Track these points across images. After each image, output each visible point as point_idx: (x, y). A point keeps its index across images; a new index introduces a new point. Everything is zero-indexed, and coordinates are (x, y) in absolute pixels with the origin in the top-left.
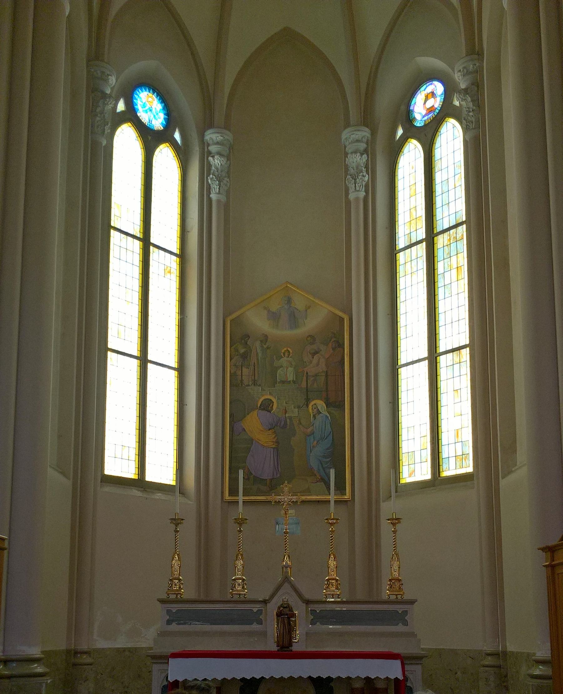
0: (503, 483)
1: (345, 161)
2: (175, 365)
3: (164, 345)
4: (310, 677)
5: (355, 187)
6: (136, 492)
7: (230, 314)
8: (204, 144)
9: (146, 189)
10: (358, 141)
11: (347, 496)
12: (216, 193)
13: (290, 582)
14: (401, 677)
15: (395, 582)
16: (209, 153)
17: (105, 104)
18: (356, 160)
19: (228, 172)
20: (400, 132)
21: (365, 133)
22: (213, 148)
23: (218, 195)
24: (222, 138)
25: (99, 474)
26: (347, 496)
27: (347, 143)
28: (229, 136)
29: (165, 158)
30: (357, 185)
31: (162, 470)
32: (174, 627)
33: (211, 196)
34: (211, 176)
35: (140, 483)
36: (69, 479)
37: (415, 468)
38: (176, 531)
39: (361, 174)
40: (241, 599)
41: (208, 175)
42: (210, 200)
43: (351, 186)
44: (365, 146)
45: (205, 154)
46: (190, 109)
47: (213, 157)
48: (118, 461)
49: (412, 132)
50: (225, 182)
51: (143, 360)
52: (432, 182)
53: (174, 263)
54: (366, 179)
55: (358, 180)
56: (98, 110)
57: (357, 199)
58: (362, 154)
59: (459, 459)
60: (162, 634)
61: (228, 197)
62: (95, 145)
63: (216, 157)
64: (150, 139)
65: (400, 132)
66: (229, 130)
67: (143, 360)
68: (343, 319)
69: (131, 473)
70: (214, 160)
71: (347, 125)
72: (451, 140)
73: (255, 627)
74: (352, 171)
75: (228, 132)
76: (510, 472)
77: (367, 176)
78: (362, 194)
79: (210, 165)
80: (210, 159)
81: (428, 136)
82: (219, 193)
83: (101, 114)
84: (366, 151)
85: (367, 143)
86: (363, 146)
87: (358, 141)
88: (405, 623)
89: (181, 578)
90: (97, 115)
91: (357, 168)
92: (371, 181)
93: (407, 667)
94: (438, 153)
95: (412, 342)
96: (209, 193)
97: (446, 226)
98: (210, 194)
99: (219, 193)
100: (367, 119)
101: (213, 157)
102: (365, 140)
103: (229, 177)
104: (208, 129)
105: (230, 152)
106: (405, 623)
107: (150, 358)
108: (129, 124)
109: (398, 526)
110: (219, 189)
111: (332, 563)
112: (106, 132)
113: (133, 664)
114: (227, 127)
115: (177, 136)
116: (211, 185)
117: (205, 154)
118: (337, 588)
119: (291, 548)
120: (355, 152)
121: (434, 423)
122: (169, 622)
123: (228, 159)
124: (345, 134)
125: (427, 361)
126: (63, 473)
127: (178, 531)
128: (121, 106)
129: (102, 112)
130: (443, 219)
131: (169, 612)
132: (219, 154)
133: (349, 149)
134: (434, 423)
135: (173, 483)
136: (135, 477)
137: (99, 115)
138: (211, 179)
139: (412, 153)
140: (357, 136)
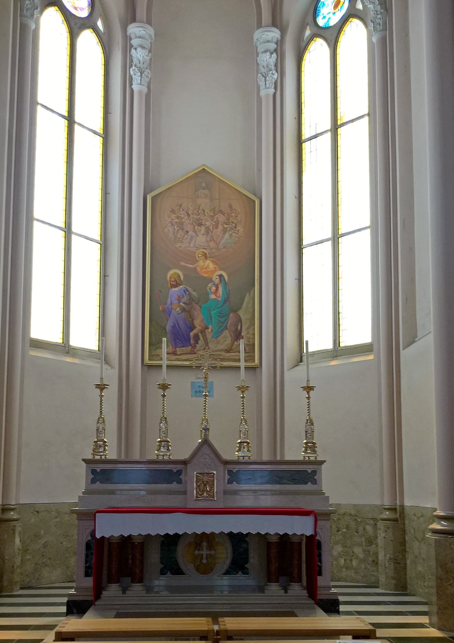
3: (88, 218)
5: (266, 84)
8: (127, 39)
9: (69, 71)
10: (268, 41)
13: (211, 446)
16: (131, 46)
18: (267, 60)
19: (150, 65)
21: (275, 34)
22: (135, 42)
23: (140, 86)
24: (144, 32)
28: (151, 31)
29: (88, 41)
30: (267, 82)
32: (98, 485)
33: (133, 87)
34: (134, 67)
36: (112, 367)
37: (318, 338)
38: (101, 396)
39: (271, 72)
41: (131, 66)
43: (262, 84)
44: (275, 46)
45: (127, 47)
47: (136, 49)
48: (44, 325)
52: (337, 80)
54: (275, 76)
55: (267, 78)
59: (359, 329)
60: (87, 492)
61: (149, 87)
62: (24, 28)
64: (75, 26)
65: (308, 33)
66: (151, 26)
68: (255, 201)
69: (57, 338)
70: (136, 51)
71: (259, 25)
72: (356, 39)
73: (174, 486)
74: (263, 70)
77: (276, 74)
79: (131, 56)
81: (332, 36)
82: (141, 84)
84: (276, 50)
85: (277, 43)
86: (273, 46)
87: (268, 41)
88: (315, 482)
89: (105, 440)
91: (267, 66)
93: (319, 523)
95: (316, 224)
96: (131, 84)
99: (141, 84)
100: (276, 22)
101: (136, 49)
102: (275, 40)
104: (130, 23)
108: (56, 8)
109: (311, 392)
110: (141, 80)
114: (149, 22)
115: (100, 24)
116: (133, 77)
119: (199, 412)
120: (265, 52)
121: (336, 296)
127: (103, 396)
130: (344, 114)
132: (143, 47)
134: (336, 296)
140: (268, 36)
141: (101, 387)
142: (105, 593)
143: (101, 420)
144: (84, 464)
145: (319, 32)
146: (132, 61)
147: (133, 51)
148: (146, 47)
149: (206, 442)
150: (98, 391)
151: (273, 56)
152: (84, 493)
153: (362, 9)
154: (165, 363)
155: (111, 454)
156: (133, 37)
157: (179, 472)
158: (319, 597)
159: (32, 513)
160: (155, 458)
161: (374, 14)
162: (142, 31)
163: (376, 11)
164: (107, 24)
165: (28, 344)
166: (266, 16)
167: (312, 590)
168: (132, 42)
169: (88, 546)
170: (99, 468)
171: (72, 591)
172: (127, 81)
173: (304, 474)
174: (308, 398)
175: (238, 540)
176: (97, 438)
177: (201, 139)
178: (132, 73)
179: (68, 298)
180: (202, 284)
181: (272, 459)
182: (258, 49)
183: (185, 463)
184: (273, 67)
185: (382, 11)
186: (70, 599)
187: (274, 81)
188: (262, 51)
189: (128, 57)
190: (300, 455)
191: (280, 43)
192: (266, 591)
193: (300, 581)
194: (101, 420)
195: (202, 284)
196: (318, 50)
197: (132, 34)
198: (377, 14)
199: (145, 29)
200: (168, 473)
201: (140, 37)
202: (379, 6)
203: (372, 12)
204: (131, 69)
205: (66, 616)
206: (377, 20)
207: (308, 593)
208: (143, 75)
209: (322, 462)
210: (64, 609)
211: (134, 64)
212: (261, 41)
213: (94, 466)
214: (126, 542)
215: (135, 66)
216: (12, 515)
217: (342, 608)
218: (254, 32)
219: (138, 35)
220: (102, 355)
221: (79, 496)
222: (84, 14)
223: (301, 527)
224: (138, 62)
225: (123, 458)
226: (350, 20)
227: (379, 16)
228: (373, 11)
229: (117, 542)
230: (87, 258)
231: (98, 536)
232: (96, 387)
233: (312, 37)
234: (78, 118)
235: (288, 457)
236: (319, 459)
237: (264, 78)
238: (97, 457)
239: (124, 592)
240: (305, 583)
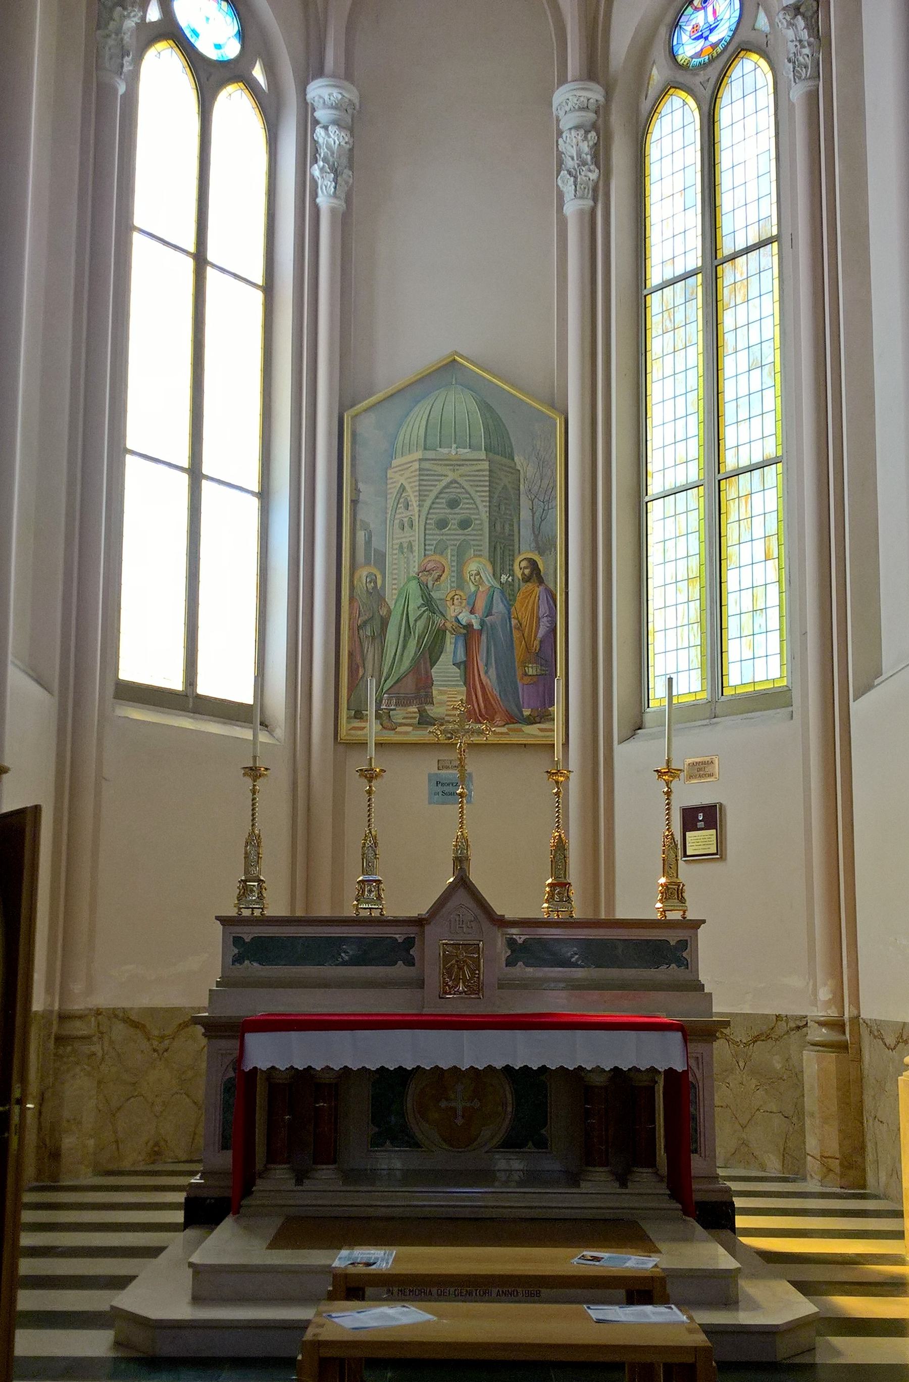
0: (855, 707)
3: (234, 449)
4: (508, 1069)
5: (576, 190)
8: (306, 110)
12: (330, 196)
14: (679, 1068)
15: (791, 25)
16: (316, 122)
17: (123, 18)
22: (322, 114)
23: (335, 201)
27: (561, 113)
29: (235, 106)
31: (228, 677)
33: (318, 200)
35: (187, 701)
37: (674, 664)
38: (254, 792)
41: (315, 161)
43: (568, 189)
45: (307, 122)
48: (146, 654)
49: (682, 77)
50: (344, 176)
52: (719, 167)
56: (112, 26)
64: (209, 77)
72: (751, 101)
73: (399, 970)
74: (570, 164)
76: (869, 687)
77: (597, 171)
79: (315, 142)
81: (706, 87)
82: (335, 195)
83: (117, 34)
84: (594, 126)
88: (683, 963)
90: (108, 36)
94: (725, 115)
96: (315, 195)
97: (741, 245)
98: (316, 196)
101: (326, 128)
102: (592, 107)
103: (351, 167)
105: (352, 119)
107: (206, 470)
110: (335, 188)
112: (125, 69)
115: (258, 73)
116: (320, 182)
117: (307, 122)
123: (351, 130)
126: (39, 681)
128: (154, 14)
129: (118, 31)
130: (737, 229)
131: (237, 941)
135: (250, 701)
137: (113, 36)
138: (322, 170)
139: (678, 114)
141: (253, 772)
142: (260, 1185)
143: (254, 841)
144: (219, 926)
145: (681, 77)
147: (319, 131)
149: (463, 883)
150: (249, 781)
151: (589, 136)
152: (218, 984)
155: (277, 905)
157: (409, 942)
158: (697, 1197)
160: (353, 913)
161: (796, 46)
163: (800, 41)
164: (271, 71)
165: (110, 690)
167: (679, 1183)
168: (317, 114)
169: (228, 1088)
170: (248, 934)
171: (196, 1180)
173: (665, 949)
174: (668, 794)
175: (528, 1082)
176: (245, 874)
177: (453, 301)
179: (198, 593)
181: (590, 916)
182: (561, 123)
183: (419, 922)
184: (589, 157)
185: (812, 39)
186: (192, 1195)
187: (591, 184)
188: (570, 125)
190: (655, 909)
191: (602, 110)
192: (583, 1184)
193: (651, 1162)
194: (254, 841)
196: (674, 130)
197: (316, 99)
198: (803, 47)
200: (386, 945)
203: (789, 43)
205: (185, 1229)
206: (801, 58)
207: (668, 1187)
209: (697, 924)
210: (179, 1217)
213: (239, 930)
214: (304, 1080)
216: (79, 1028)
217: (740, 1222)
218: (553, 92)
221: (210, 990)
222: (232, 50)
223: (663, 1054)
225: (299, 913)
227: (806, 51)
229: (595, 1166)
231: (248, 1067)
232: (244, 775)
234: (212, 255)
235: (621, 913)
236: (690, 916)
238: (246, 913)
239: (299, 1181)
240: (664, 1170)
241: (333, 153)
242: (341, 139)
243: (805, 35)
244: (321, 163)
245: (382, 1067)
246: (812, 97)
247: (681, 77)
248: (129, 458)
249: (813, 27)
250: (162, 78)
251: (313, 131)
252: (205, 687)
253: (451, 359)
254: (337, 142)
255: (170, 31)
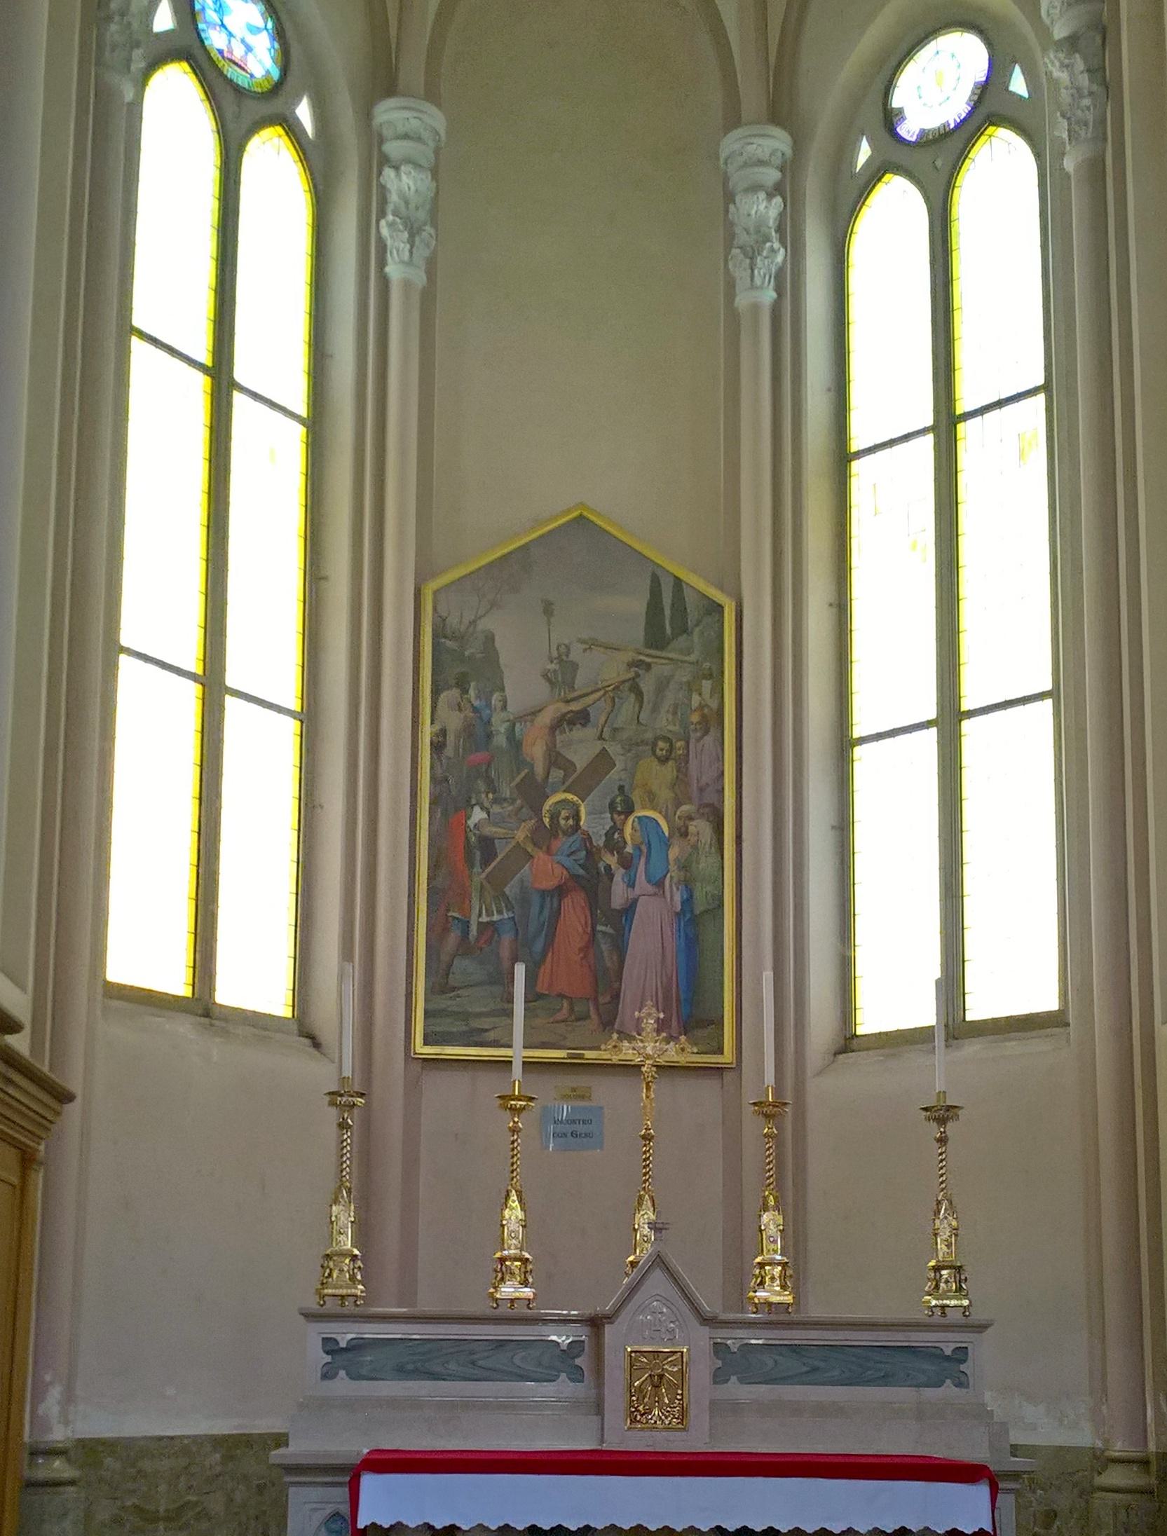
1: (727, 211)
2: (295, 705)
3: (267, 651)
6: (184, 1027)
7: (434, 575)
8: (373, 140)
9: (220, 238)
10: (761, 163)
11: (728, 1057)
12: (402, 262)
16: (384, 160)
20: (864, 152)
21: (777, 142)
22: (393, 148)
25: (100, 984)
26: (728, 1057)
28: (435, 119)
29: (272, 163)
32: (343, 1386)
33: (387, 269)
34: (390, 217)
36: (23, 988)
37: (892, 995)
39: (768, 244)
40: (345, 1311)
41: (382, 214)
42: (384, 282)
43: (741, 274)
45: (376, 160)
46: (338, 45)
48: (142, 947)
51: (213, 684)
52: (946, 300)
53: (291, 441)
54: (780, 258)
57: (755, 308)
58: (770, 196)
63: (403, 168)
64: (238, 112)
65: (864, 152)
66: (439, 106)
67: (213, 684)
68: (719, 608)
69: (174, 980)
71: (733, 120)
74: (742, 238)
75: (433, 110)
77: (782, 250)
78: (770, 295)
79: (383, 190)
80: (389, 173)
81: (936, 164)
82: (410, 263)
84: (778, 189)
85: (782, 169)
86: (771, 176)
87: (761, 163)
92: (792, 264)
95: (889, 675)
96: (382, 263)
99: (410, 263)
100: (781, 111)
102: (777, 161)
103: (434, 225)
106: (961, 1382)
107: (231, 680)
110: (411, 252)
111: (514, 1213)
113: (249, 1477)
114: (432, 95)
115: (304, 112)
116: (389, 242)
118: (525, 1283)
121: (947, 886)
122: (328, 1374)
124: (730, 143)
125: (934, 730)
128: (164, 20)
132: (417, 166)
133: (738, 179)
135: (287, 1013)
136: (185, 991)
138: (391, 225)
145: (899, 155)
146: (383, 201)
147: (389, 173)
148: (423, 162)
151: (774, 201)
153: (1026, 95)
154: (517, 1053)
156: (386, 132)
159: (531, 1099)
162: (413, 121)
165: (100, 990)
166: (752, 97)
172: (372, 254)
177: (580, 451)
178: (385, 231)
180: (579, 789)
189: (374, 191)
191: (792, 168)
195: (579, 789)
196: (892, 215)
198: (1081, 97)
199: (420, 115)
201: (406, 136)
202: (1086, 75)
203: (1063, 91)
204: (383, 223)
208: (417, 239)
211: (390, 208)
212: (741, 160)
215: (395, 214)
219: (401, 129)
220: (303, 1028)
224: (403, 204)
226: (987, 132)
227: (1086, 102)
228: (1066, 88)
230: (264, 757)
233: (879, 170)
237: (748, 261)
241: (407, 203)
242: (419, 183)
243: (1084, 80)
244: (390, 217)
245: (771, 1528)
246: (1095, 170)
247: (899, 155)
248: (124, 659)
249: (1096, 71)
250: (172, 108)
251: (380, 173)
252: (227, 994)
253: (576, 514)
254: (413, 188)
255: (187, 46)
